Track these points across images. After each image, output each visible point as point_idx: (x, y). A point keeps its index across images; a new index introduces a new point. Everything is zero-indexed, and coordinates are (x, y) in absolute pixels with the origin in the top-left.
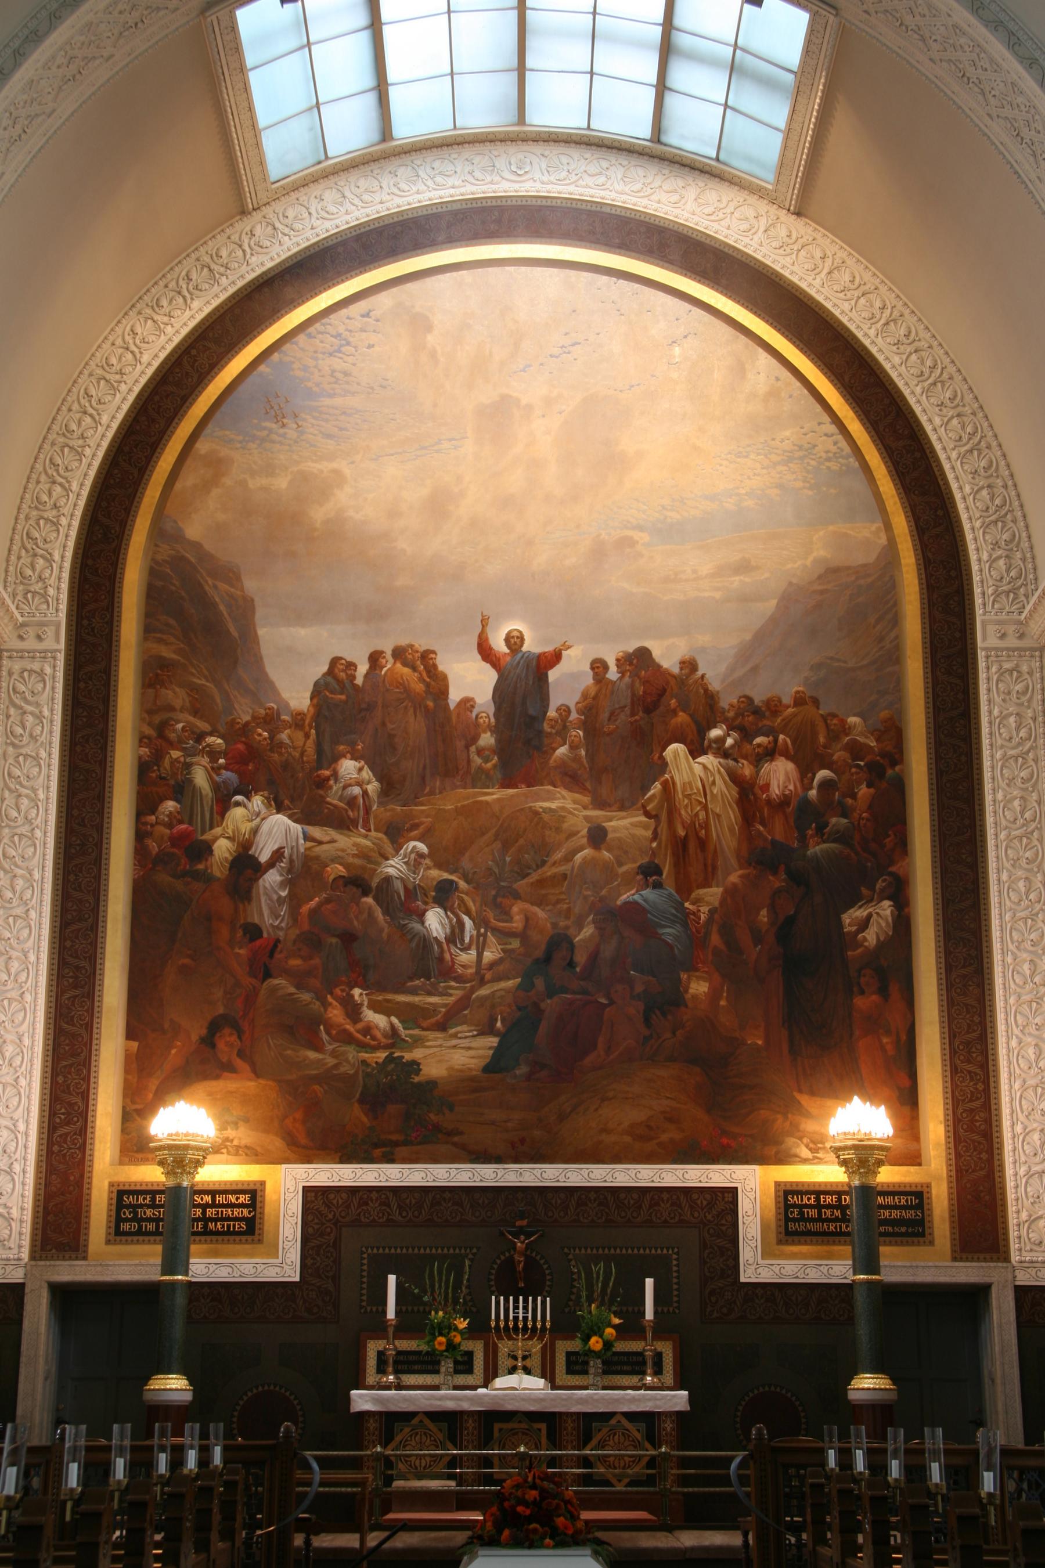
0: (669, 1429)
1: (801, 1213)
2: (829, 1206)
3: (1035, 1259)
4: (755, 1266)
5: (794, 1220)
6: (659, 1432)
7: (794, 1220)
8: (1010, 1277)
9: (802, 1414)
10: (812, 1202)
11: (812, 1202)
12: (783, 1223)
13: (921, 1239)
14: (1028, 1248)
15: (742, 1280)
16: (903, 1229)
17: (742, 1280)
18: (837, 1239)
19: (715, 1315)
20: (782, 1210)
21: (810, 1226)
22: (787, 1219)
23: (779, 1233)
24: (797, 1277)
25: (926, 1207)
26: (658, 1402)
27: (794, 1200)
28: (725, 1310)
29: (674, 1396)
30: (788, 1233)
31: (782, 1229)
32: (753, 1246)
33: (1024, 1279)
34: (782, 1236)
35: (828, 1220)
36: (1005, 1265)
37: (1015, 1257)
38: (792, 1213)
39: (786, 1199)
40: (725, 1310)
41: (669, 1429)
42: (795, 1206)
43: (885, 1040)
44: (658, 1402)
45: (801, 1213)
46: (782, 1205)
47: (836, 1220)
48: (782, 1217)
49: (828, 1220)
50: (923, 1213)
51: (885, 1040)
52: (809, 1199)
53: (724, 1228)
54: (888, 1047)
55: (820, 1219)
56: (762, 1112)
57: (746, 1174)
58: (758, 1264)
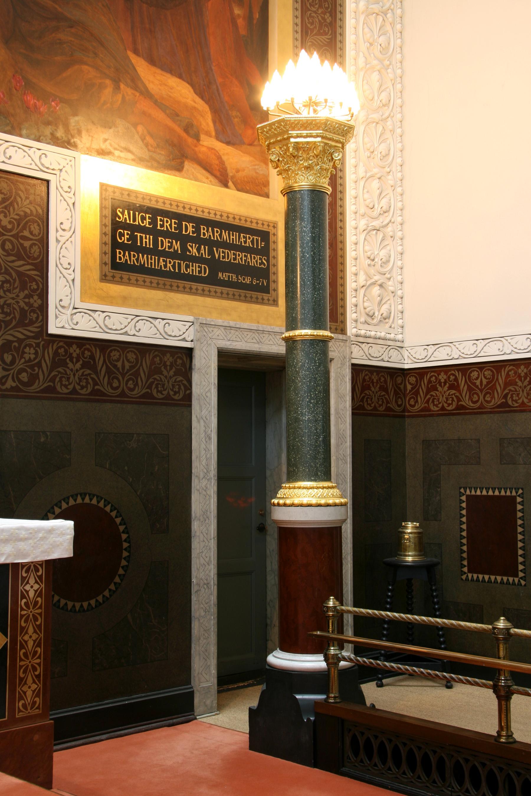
0: (32, 594)
1: (133, 238)
2: (167, 234)
3: (368, 333)
4: (70, 311)
5: (124, 247)
6: (15, 602)
7: (124, 247)
8: (348, 352)
9: (124, 536)
10: (146, 223)
11: (146, 223)
12: (108, 249)
13: (266, 296)
14: (362, 320)
15: (52, 329)
16: (248, 280)
17: (52, 329)
18: (175, 282)
19: (10, 383)
20: (109, 229)
21: (143, 259)
22: (115, 245)
23: (103, 264)
24: (126, 333)
25: (272, 253)
26: (22, 545)
27: (124, 217)
28: (24, 377)
29: (51, 531)
30: (115, 265)
31: (108, 259)
32: (70, 278)
33: (361, 356)
34: (108, 269)
35: (164, 254)
36: (341, 336)
37: (351, 330)
38: (122, 235)
39: (114, 215)
40: (24, 377)
41: (32, 594)
42: (125, 226)
43: (237, 11)
44: (22, 545)
45: (133, 238)
46: (108, 221)
47: (174, 255)
48: (108, 239)
49: (164, 254)
50: (268, 261)
51: (237, 11)
52: (143, 219)
53: (27, 244)
54: (240, 22)
55: (154, 251)
56: (85, 68)
57: (63, 163)
58: (78, 306)
